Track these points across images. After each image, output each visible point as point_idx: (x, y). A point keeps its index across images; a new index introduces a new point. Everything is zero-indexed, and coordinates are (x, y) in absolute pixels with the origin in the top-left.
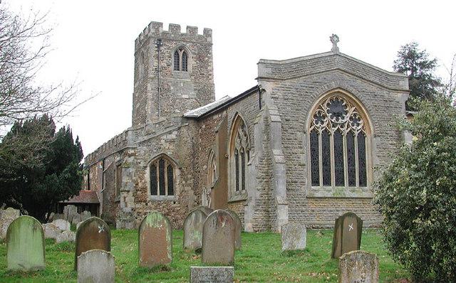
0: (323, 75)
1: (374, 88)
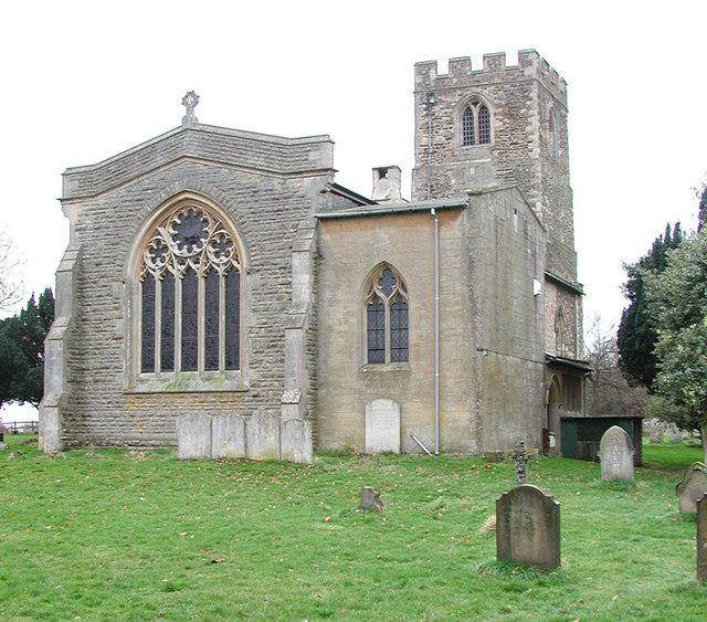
0: (160, 174)
1: (255, 179)
